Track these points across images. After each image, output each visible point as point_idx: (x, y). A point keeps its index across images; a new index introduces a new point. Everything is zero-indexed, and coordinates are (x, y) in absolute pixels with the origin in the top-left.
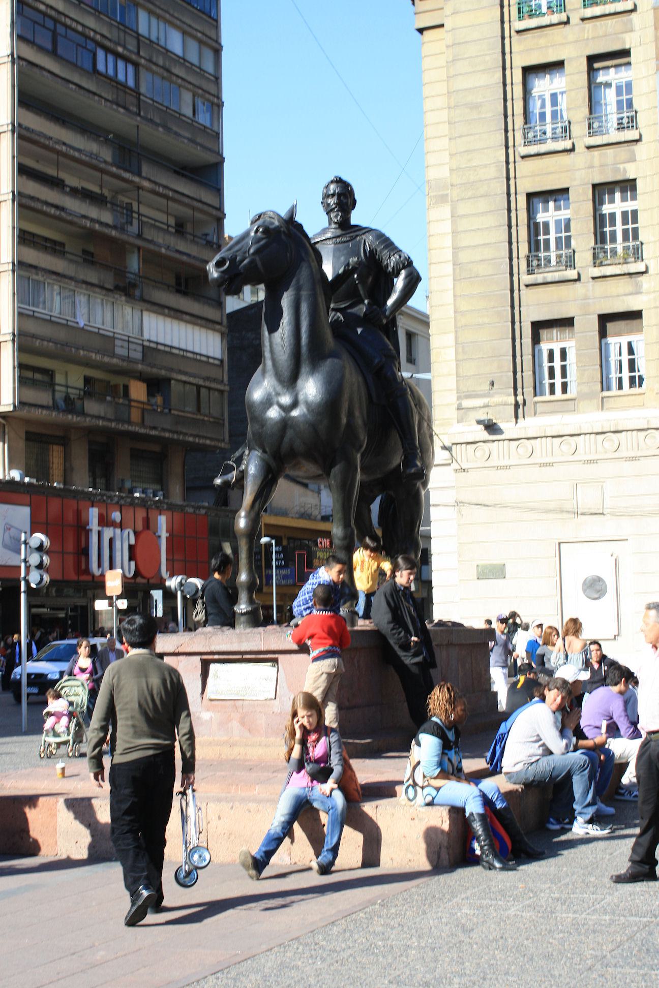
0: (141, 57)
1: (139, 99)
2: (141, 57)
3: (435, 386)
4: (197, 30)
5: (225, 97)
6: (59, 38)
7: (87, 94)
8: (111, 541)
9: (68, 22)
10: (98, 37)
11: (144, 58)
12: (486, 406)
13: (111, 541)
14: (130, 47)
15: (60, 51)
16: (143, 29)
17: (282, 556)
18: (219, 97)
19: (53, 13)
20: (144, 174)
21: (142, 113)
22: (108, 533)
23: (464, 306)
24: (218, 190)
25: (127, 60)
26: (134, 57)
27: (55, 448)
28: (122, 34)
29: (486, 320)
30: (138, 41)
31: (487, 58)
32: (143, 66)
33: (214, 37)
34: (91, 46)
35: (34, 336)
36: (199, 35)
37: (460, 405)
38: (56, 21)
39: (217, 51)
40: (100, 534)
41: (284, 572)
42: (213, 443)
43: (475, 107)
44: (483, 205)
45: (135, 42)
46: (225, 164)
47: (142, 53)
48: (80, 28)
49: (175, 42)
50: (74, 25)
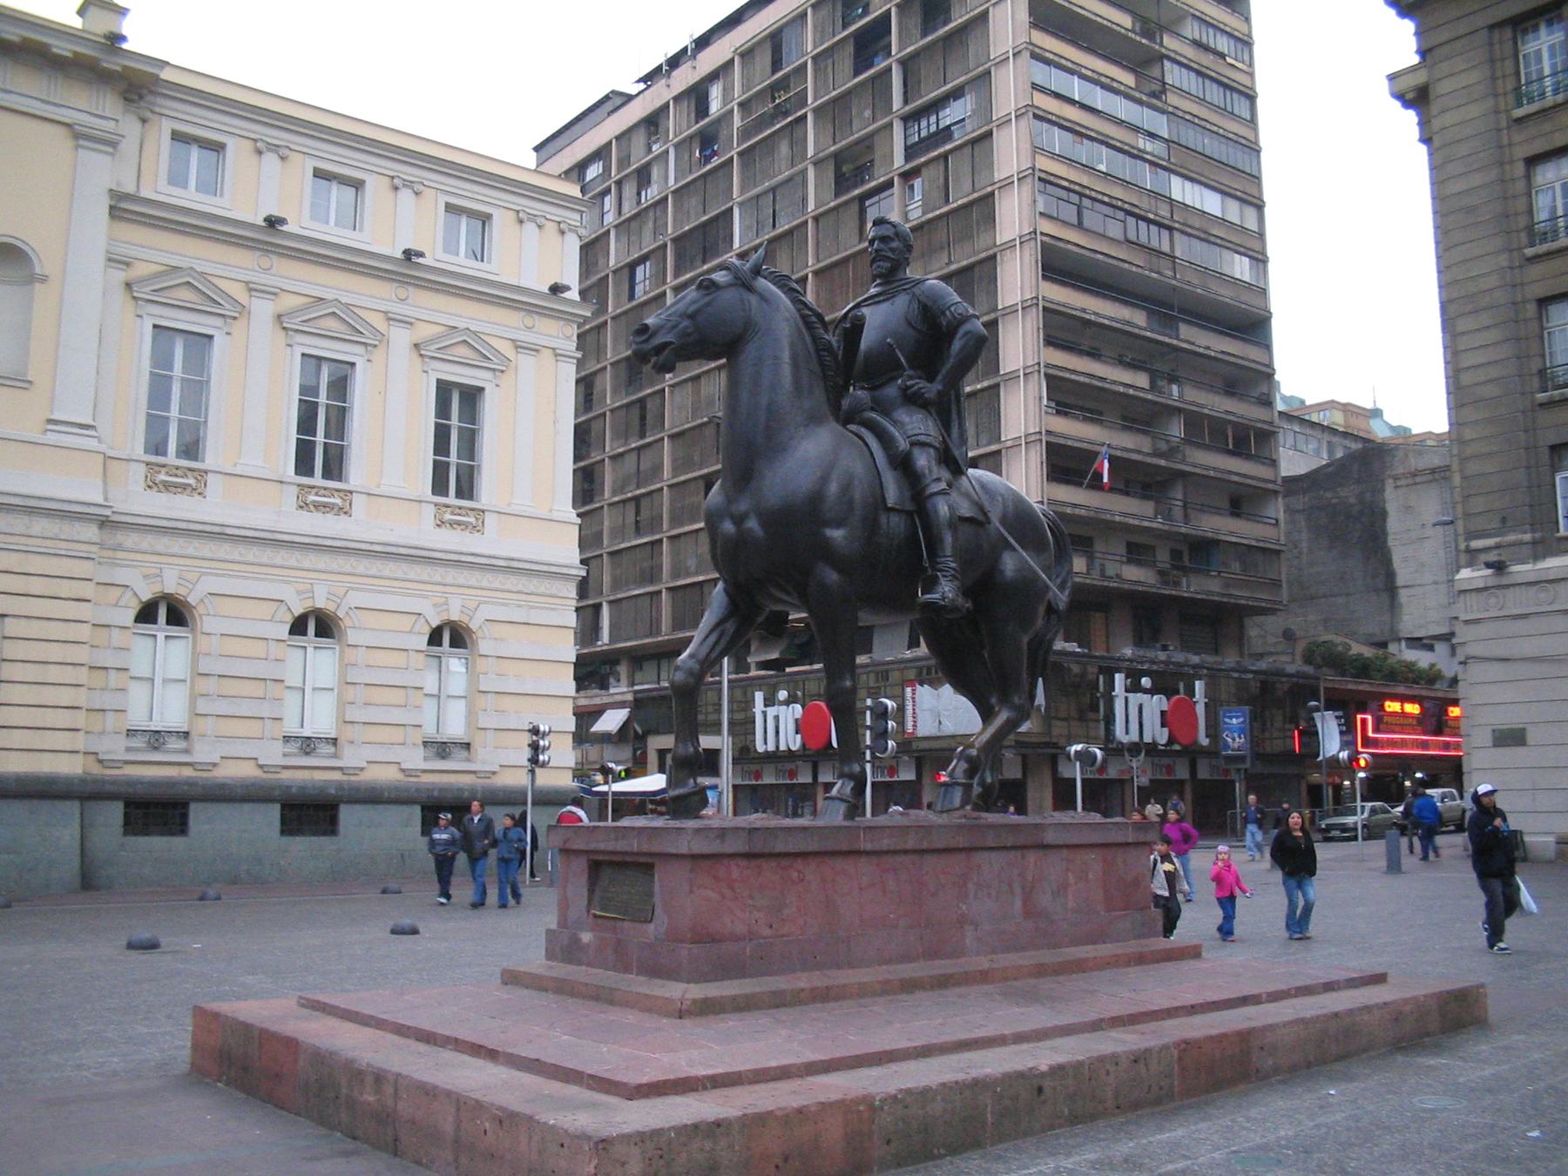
0: (1175, 221)
1: (1174, 262)
2: (1175, 221)
3: (146, 407)
4: (1236, 189)
5: (1270, 252)
6: (1085, 211)
7: (568, 133)
8: (777, 718)
9: (1094, 194)
10: (1126, 206)
11: (1178, 222)
12: (1498, 546)
13: (777, 718)
14: (1162, 213)
15: (1086, 223)
16: (1176, 195)
17: (1343, 720)
18: (1264, 253)
19: (1077, 188)
20: (1182, 337)
21: (1178, 276)
22: (771, 711)
23: (1468, 434)
24: (1267, 347)
25: (1160, 225)
26: (1170, 223)
27: (1098, 615)
28: (1153, 201)
29: (1495, 448)
30: (1172, 205)
31: (1481, 155)
32: (1177, 229)
33: (1256, 194)
34: (1120, 215)
35: (1064, 504)
36: (1239, 194)
37: (1467, 546)
38: (1081, 195)
39: (1260, 207)
40: (765, 713)
41: (1345, 738)
42: (1269, 606)
43: (1470, 210)
44: (1485, 319)
45: (1168, 208)
46: (1273, 320)
47: (1175, 218)
48: (1106, 199)
49: (1211, 203)
50: (1100, 197)
